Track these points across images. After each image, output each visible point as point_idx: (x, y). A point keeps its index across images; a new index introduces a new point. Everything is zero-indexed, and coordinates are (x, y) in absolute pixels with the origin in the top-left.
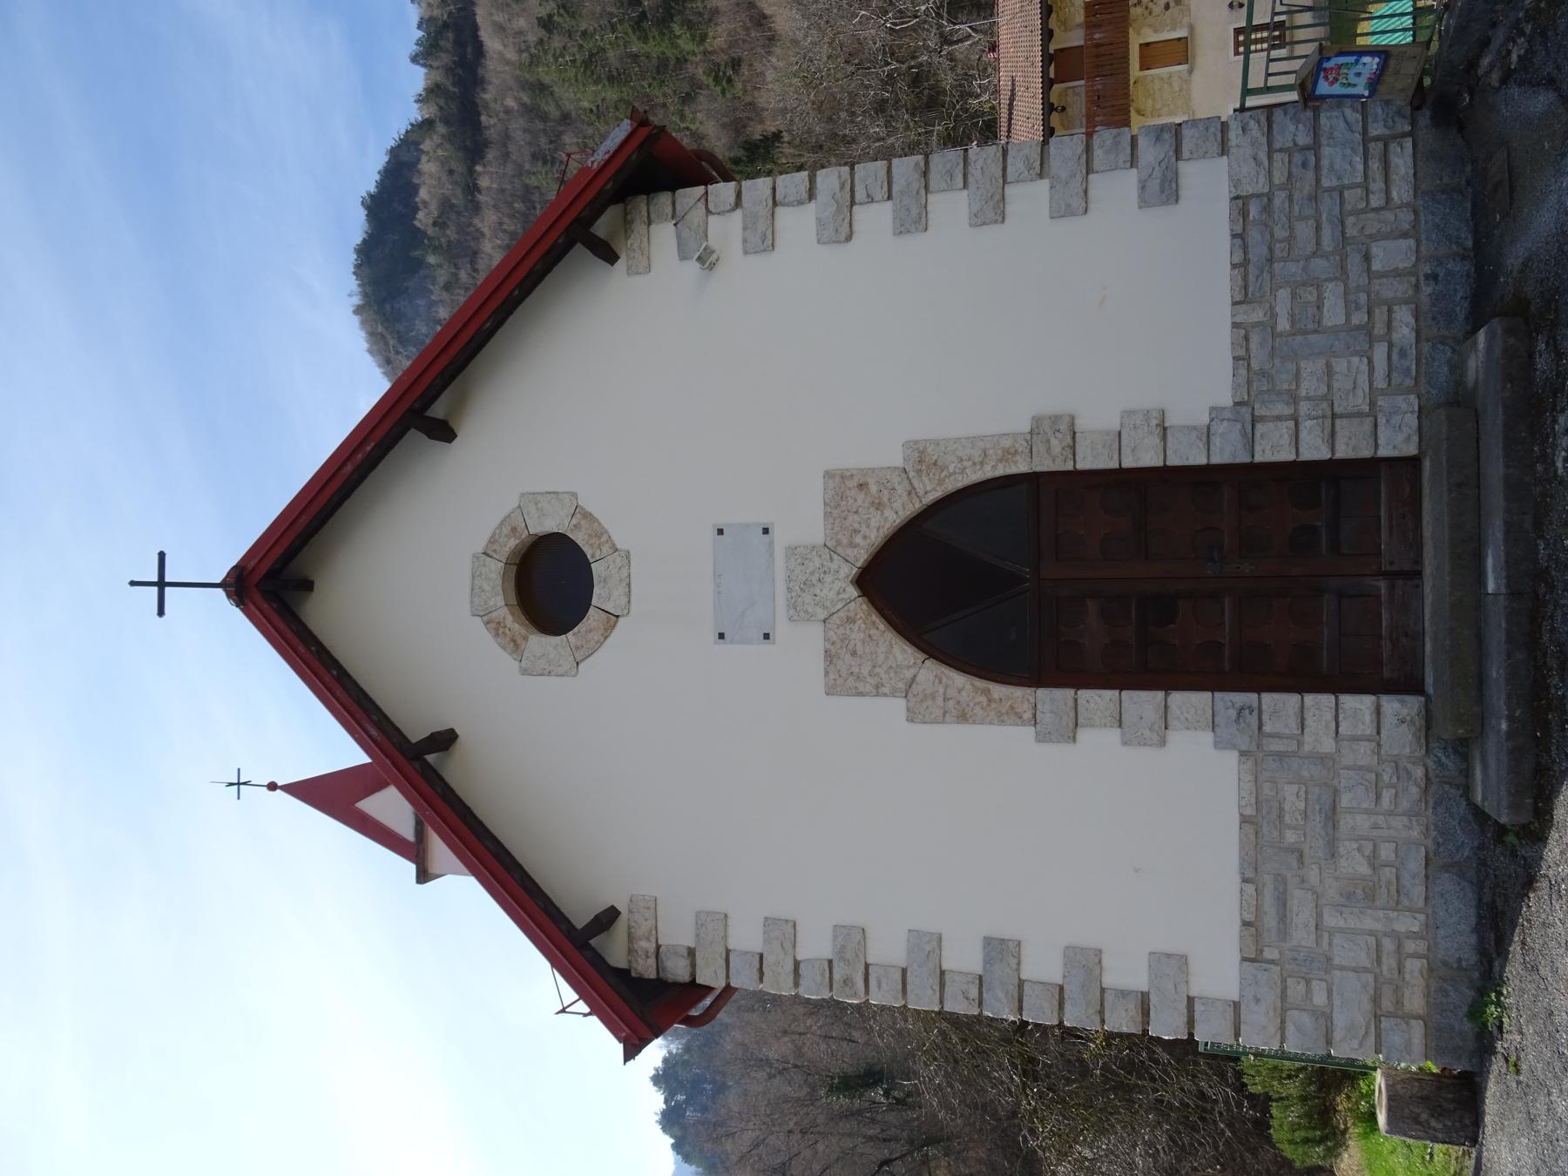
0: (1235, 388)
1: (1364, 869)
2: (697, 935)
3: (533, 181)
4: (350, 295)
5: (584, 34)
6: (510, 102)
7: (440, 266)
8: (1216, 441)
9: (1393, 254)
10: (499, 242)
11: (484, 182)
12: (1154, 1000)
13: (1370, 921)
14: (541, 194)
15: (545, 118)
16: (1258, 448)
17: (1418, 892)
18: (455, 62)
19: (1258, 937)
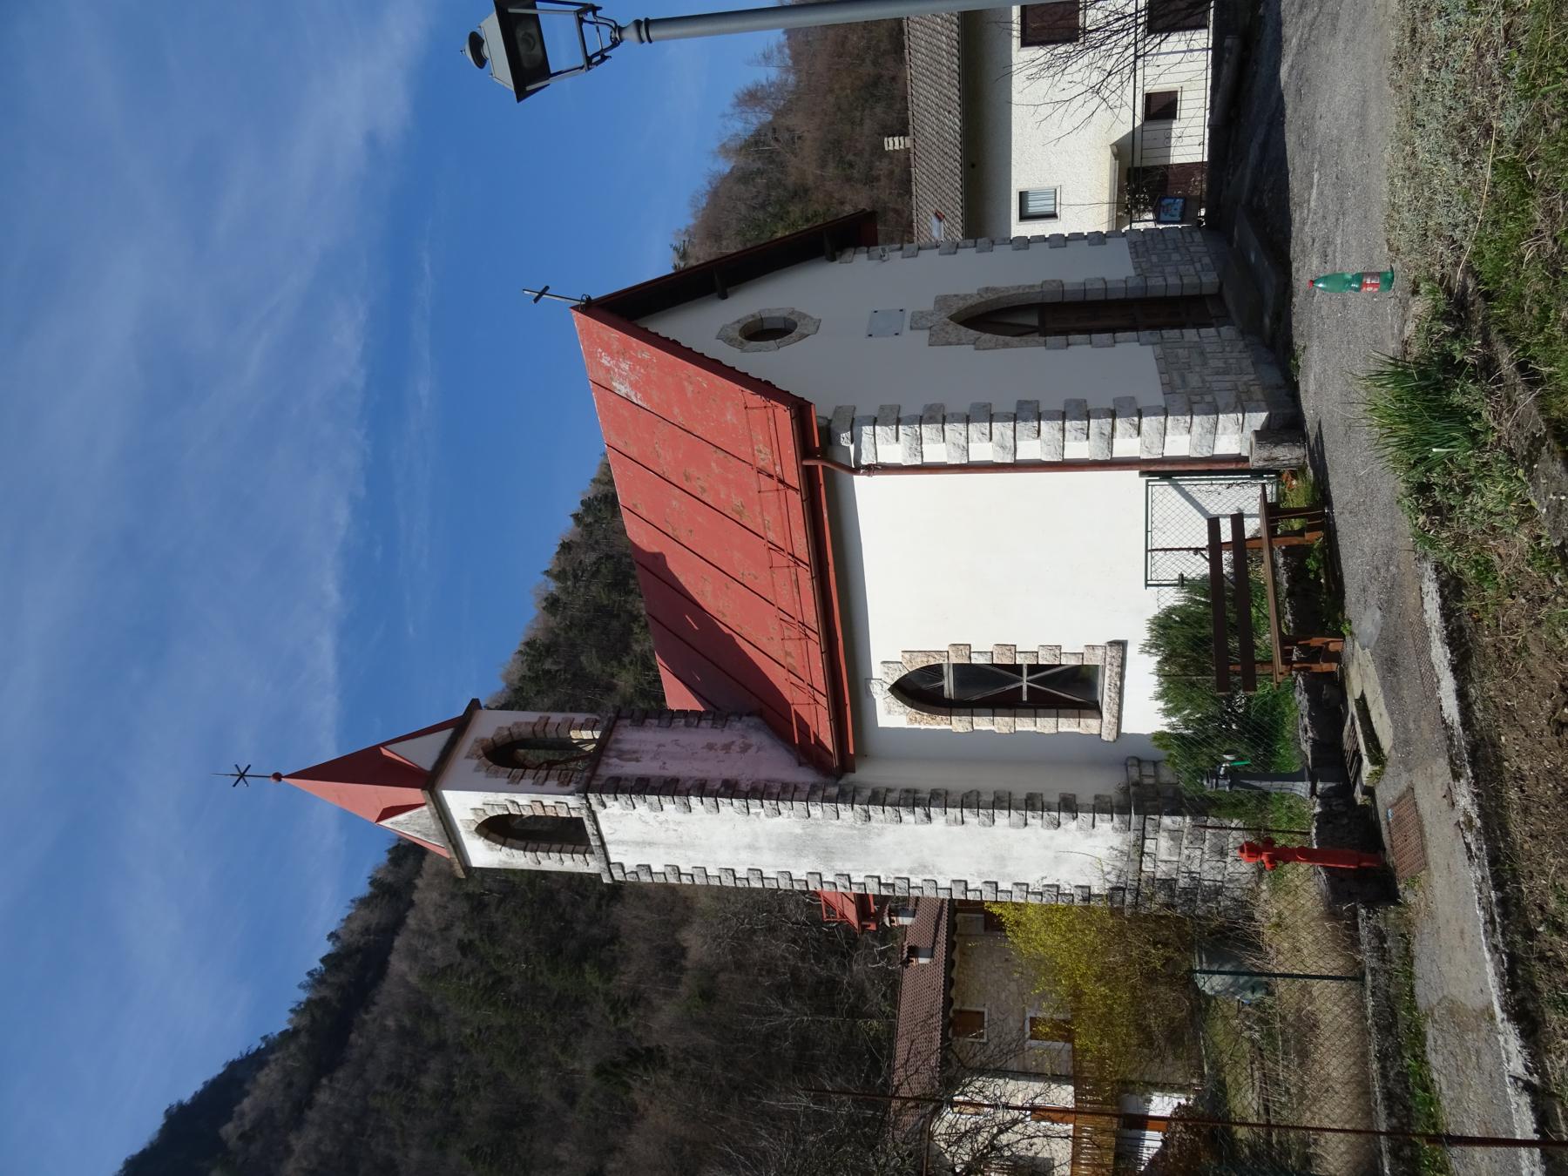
3: (375, 1102)
5: (499, 958)
6: (390, 1022)
10: (305, 1164)
11: (323, 1097)
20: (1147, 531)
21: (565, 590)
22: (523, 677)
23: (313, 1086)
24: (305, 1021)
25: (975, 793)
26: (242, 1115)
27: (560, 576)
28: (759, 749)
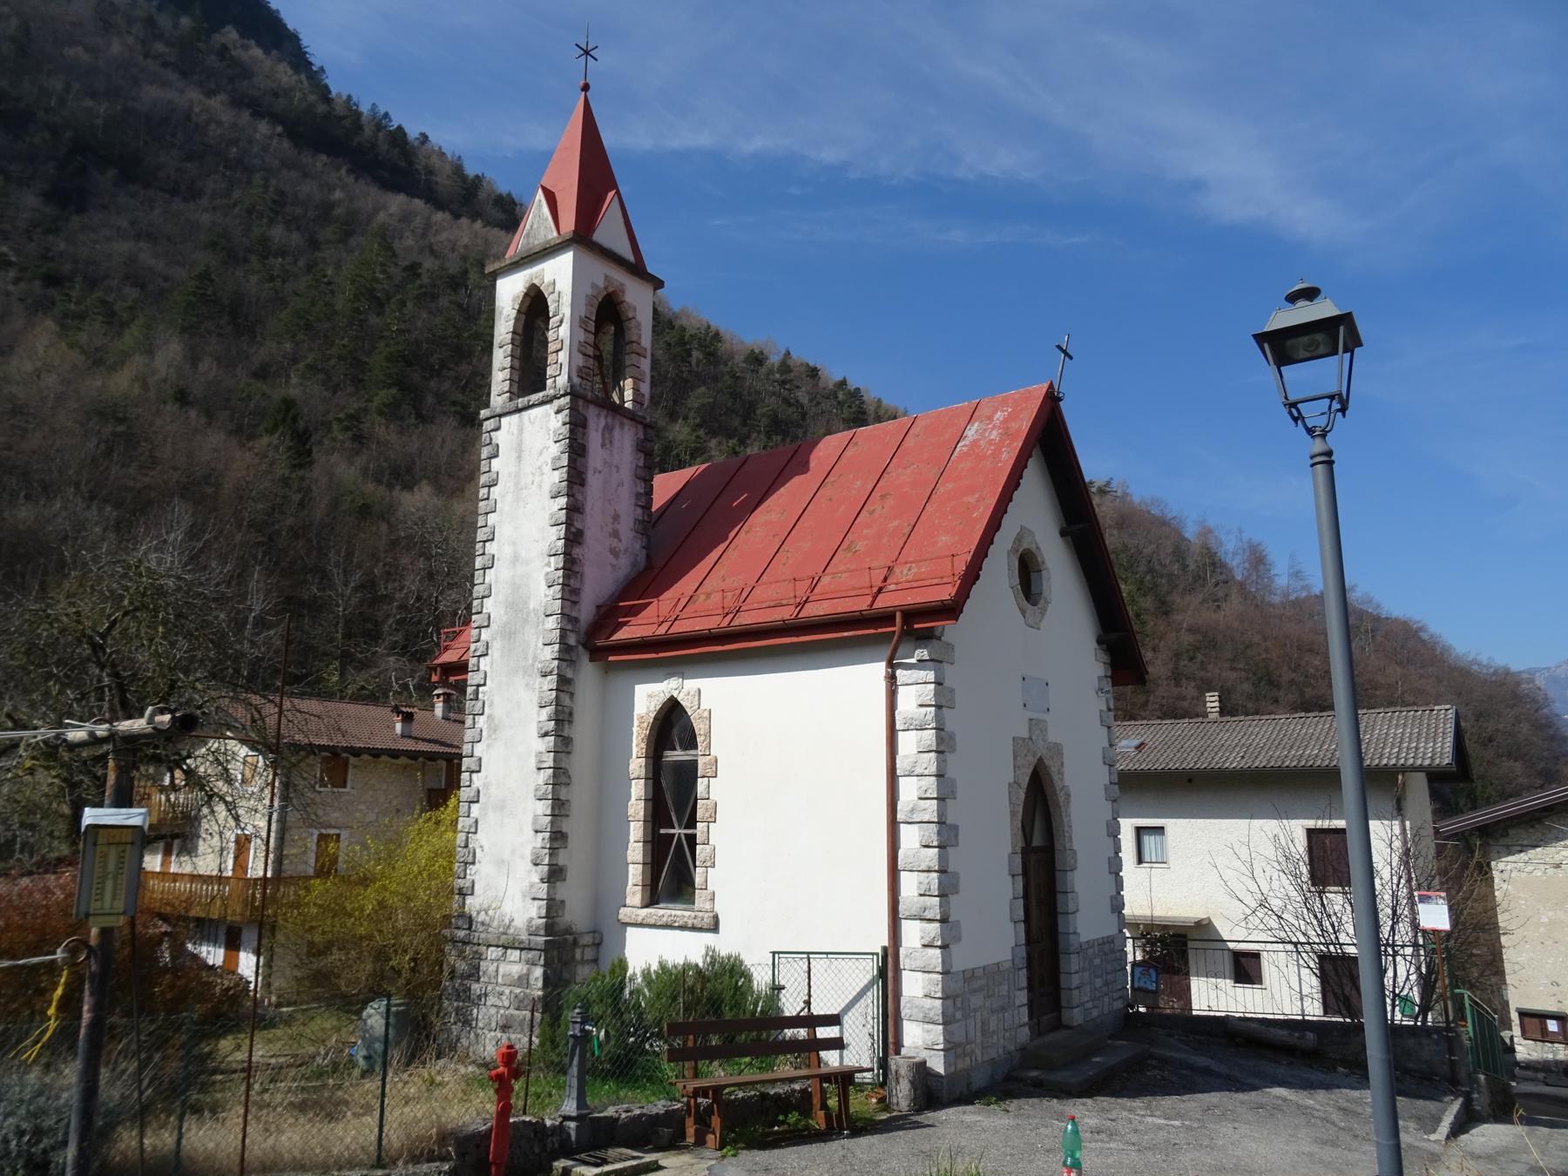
3: (257, 179)
6: (338, 195)
10: (197, 110)
11: (263, 127)
20: (827, 953)
21: (771, 372)
22: (683, 329)
23: (275, 118)
24: (340, 110)
26: (246, 48)
27: (785, 367)
28: (613, 566)
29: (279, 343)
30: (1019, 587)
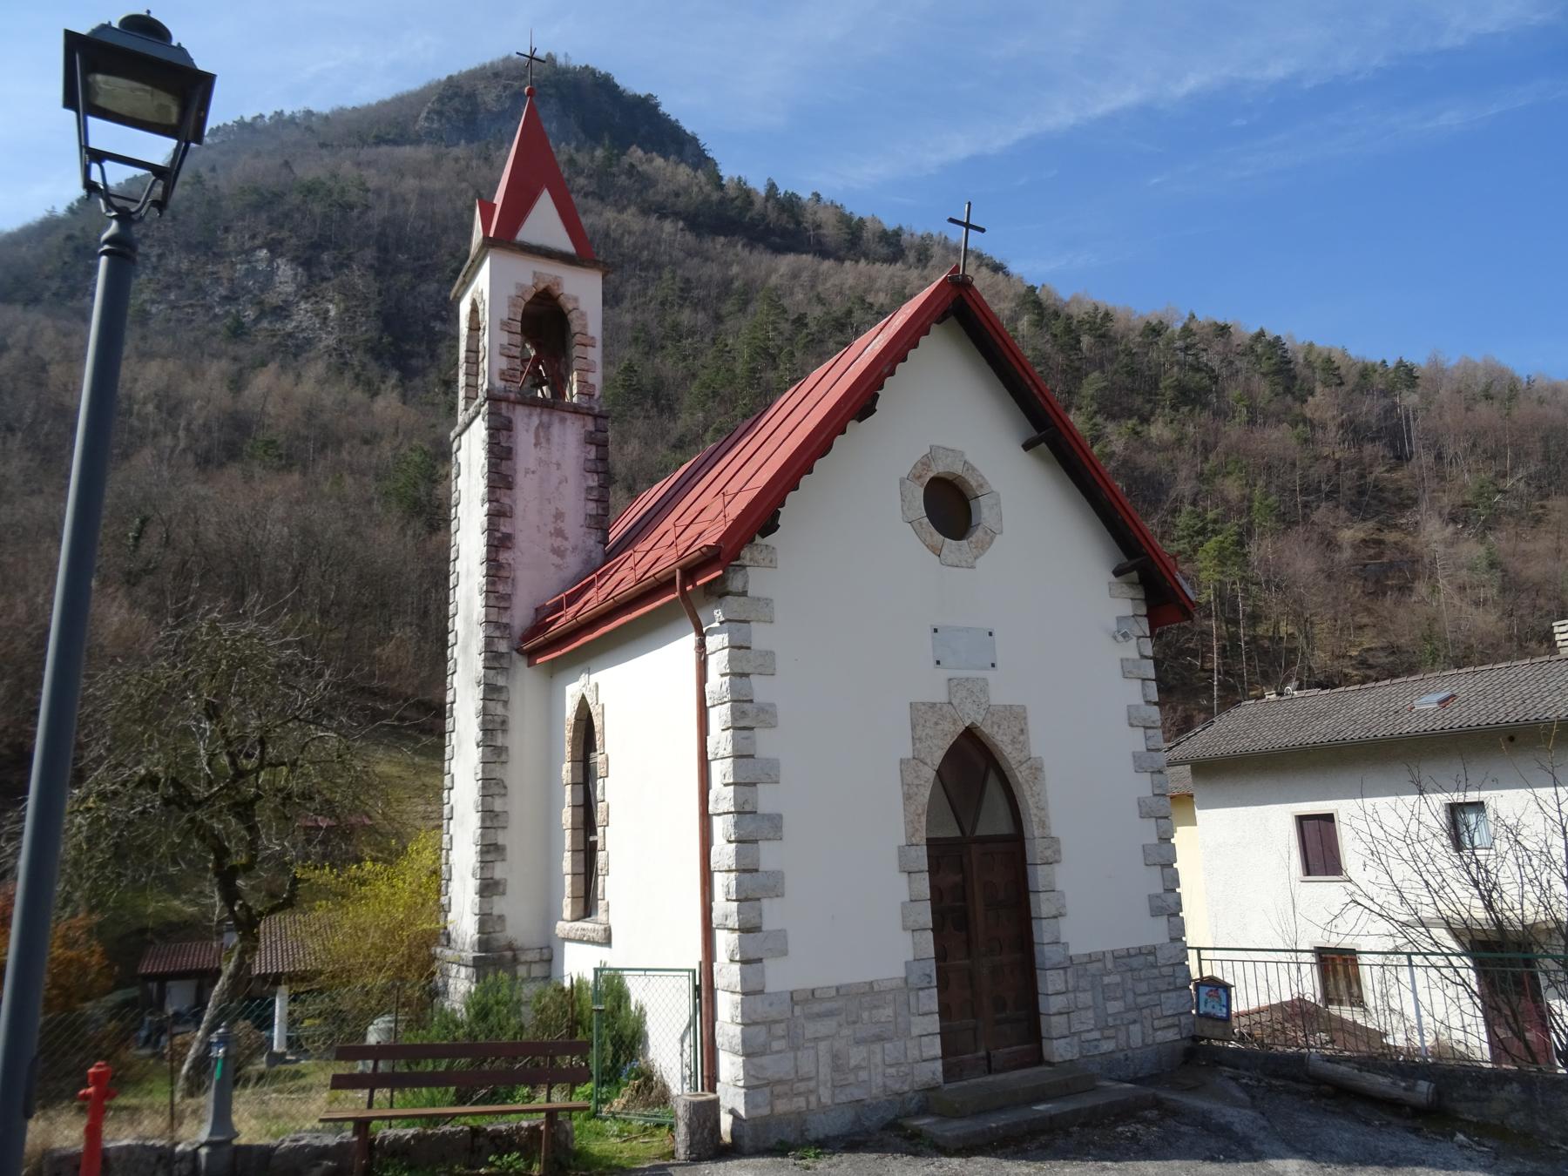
0: (1078, 956)
1: (853, 1063)
2: (759, 599)
3: (666, 275)
4: (566, 55)
5: (792, 354)
6: (735, 269)
7: (592, 159)
8: (1054, 948)
9: (1136, 1035)
10: (613, 227)
11: (668, 226)
12: (759, 935)
13: (825, 1072)
14: (654, 280)
15: (720, 298)
16: (1052, 972)
17: (842, 1098)
18: (768, 224)
19: (806, 1001)
20: (646, 970)
21: (1171, 341)
22: (1069, 317)
23: (677, 215)
24: (732, 193)
25: (503, 792)
26: (651, 161)
27: (1187, 331)
28: (558, 567)
29: (692, 414)
30: (926, 520)
